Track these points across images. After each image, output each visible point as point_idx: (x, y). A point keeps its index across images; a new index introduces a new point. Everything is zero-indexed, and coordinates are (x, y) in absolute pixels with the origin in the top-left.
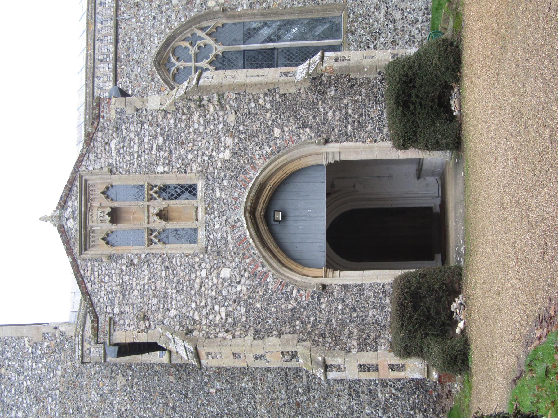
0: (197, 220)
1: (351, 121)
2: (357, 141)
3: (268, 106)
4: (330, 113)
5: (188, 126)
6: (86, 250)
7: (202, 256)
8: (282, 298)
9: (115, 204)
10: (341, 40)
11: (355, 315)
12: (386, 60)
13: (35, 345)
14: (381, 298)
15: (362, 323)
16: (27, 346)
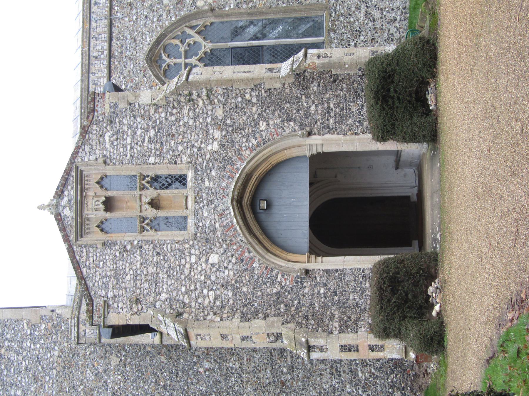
0: (187, 208)
1: (332, 114)
2: (338, 134)
3: (254, 100)
4: (313, 107)
5: (178, 120)
6: (81, 237)
7: (191, 242)
8: (267, 282)
9: (109, 194)
10: (323, 38)
11: (336, 298)
12: (366, 57)
13: (33, 327)
14: (361, 283)
15: (343, 306)
16: (26, 327)
